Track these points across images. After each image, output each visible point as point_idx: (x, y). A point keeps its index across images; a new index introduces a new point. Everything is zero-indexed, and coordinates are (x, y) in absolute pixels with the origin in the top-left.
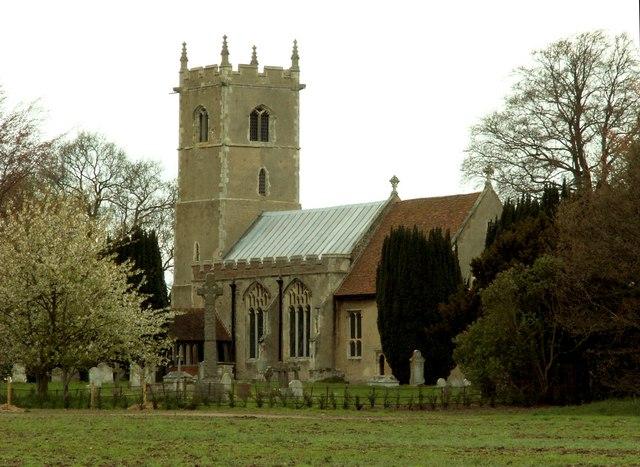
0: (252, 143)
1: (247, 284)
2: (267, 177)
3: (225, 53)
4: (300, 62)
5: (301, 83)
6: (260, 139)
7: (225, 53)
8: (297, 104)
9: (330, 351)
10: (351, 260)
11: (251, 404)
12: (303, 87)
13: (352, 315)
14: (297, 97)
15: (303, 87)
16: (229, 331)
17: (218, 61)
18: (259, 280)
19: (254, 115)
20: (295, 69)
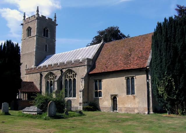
0: (43, 37)
1: (46, 73)
2: (47, 47)
3: (38, 11)
4: (56, 19)
5: (56, 24)
6: (46, 36)
7: (38, 11)
8: (55, 29)
9: (87, 95)
10: (93, 61)
11: (33, 109)
12: (57, 25)
13: (96, 81)
14: (55, 27)
15: (57, 25)
16: (39, 89)
17: (35, 13)
18: (52, 71)
19: (44, 30)
20: (55, 20)
